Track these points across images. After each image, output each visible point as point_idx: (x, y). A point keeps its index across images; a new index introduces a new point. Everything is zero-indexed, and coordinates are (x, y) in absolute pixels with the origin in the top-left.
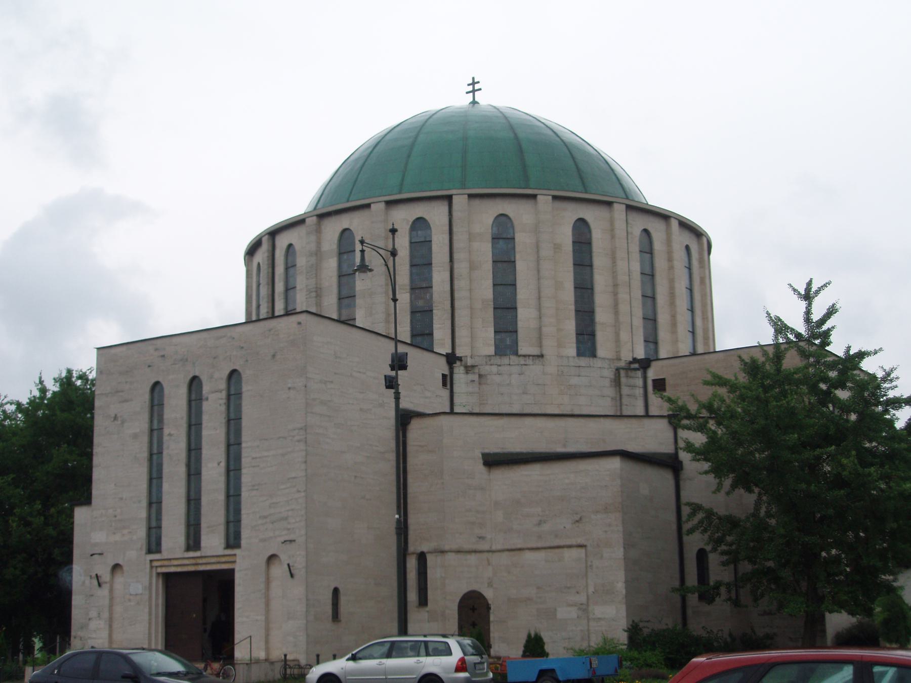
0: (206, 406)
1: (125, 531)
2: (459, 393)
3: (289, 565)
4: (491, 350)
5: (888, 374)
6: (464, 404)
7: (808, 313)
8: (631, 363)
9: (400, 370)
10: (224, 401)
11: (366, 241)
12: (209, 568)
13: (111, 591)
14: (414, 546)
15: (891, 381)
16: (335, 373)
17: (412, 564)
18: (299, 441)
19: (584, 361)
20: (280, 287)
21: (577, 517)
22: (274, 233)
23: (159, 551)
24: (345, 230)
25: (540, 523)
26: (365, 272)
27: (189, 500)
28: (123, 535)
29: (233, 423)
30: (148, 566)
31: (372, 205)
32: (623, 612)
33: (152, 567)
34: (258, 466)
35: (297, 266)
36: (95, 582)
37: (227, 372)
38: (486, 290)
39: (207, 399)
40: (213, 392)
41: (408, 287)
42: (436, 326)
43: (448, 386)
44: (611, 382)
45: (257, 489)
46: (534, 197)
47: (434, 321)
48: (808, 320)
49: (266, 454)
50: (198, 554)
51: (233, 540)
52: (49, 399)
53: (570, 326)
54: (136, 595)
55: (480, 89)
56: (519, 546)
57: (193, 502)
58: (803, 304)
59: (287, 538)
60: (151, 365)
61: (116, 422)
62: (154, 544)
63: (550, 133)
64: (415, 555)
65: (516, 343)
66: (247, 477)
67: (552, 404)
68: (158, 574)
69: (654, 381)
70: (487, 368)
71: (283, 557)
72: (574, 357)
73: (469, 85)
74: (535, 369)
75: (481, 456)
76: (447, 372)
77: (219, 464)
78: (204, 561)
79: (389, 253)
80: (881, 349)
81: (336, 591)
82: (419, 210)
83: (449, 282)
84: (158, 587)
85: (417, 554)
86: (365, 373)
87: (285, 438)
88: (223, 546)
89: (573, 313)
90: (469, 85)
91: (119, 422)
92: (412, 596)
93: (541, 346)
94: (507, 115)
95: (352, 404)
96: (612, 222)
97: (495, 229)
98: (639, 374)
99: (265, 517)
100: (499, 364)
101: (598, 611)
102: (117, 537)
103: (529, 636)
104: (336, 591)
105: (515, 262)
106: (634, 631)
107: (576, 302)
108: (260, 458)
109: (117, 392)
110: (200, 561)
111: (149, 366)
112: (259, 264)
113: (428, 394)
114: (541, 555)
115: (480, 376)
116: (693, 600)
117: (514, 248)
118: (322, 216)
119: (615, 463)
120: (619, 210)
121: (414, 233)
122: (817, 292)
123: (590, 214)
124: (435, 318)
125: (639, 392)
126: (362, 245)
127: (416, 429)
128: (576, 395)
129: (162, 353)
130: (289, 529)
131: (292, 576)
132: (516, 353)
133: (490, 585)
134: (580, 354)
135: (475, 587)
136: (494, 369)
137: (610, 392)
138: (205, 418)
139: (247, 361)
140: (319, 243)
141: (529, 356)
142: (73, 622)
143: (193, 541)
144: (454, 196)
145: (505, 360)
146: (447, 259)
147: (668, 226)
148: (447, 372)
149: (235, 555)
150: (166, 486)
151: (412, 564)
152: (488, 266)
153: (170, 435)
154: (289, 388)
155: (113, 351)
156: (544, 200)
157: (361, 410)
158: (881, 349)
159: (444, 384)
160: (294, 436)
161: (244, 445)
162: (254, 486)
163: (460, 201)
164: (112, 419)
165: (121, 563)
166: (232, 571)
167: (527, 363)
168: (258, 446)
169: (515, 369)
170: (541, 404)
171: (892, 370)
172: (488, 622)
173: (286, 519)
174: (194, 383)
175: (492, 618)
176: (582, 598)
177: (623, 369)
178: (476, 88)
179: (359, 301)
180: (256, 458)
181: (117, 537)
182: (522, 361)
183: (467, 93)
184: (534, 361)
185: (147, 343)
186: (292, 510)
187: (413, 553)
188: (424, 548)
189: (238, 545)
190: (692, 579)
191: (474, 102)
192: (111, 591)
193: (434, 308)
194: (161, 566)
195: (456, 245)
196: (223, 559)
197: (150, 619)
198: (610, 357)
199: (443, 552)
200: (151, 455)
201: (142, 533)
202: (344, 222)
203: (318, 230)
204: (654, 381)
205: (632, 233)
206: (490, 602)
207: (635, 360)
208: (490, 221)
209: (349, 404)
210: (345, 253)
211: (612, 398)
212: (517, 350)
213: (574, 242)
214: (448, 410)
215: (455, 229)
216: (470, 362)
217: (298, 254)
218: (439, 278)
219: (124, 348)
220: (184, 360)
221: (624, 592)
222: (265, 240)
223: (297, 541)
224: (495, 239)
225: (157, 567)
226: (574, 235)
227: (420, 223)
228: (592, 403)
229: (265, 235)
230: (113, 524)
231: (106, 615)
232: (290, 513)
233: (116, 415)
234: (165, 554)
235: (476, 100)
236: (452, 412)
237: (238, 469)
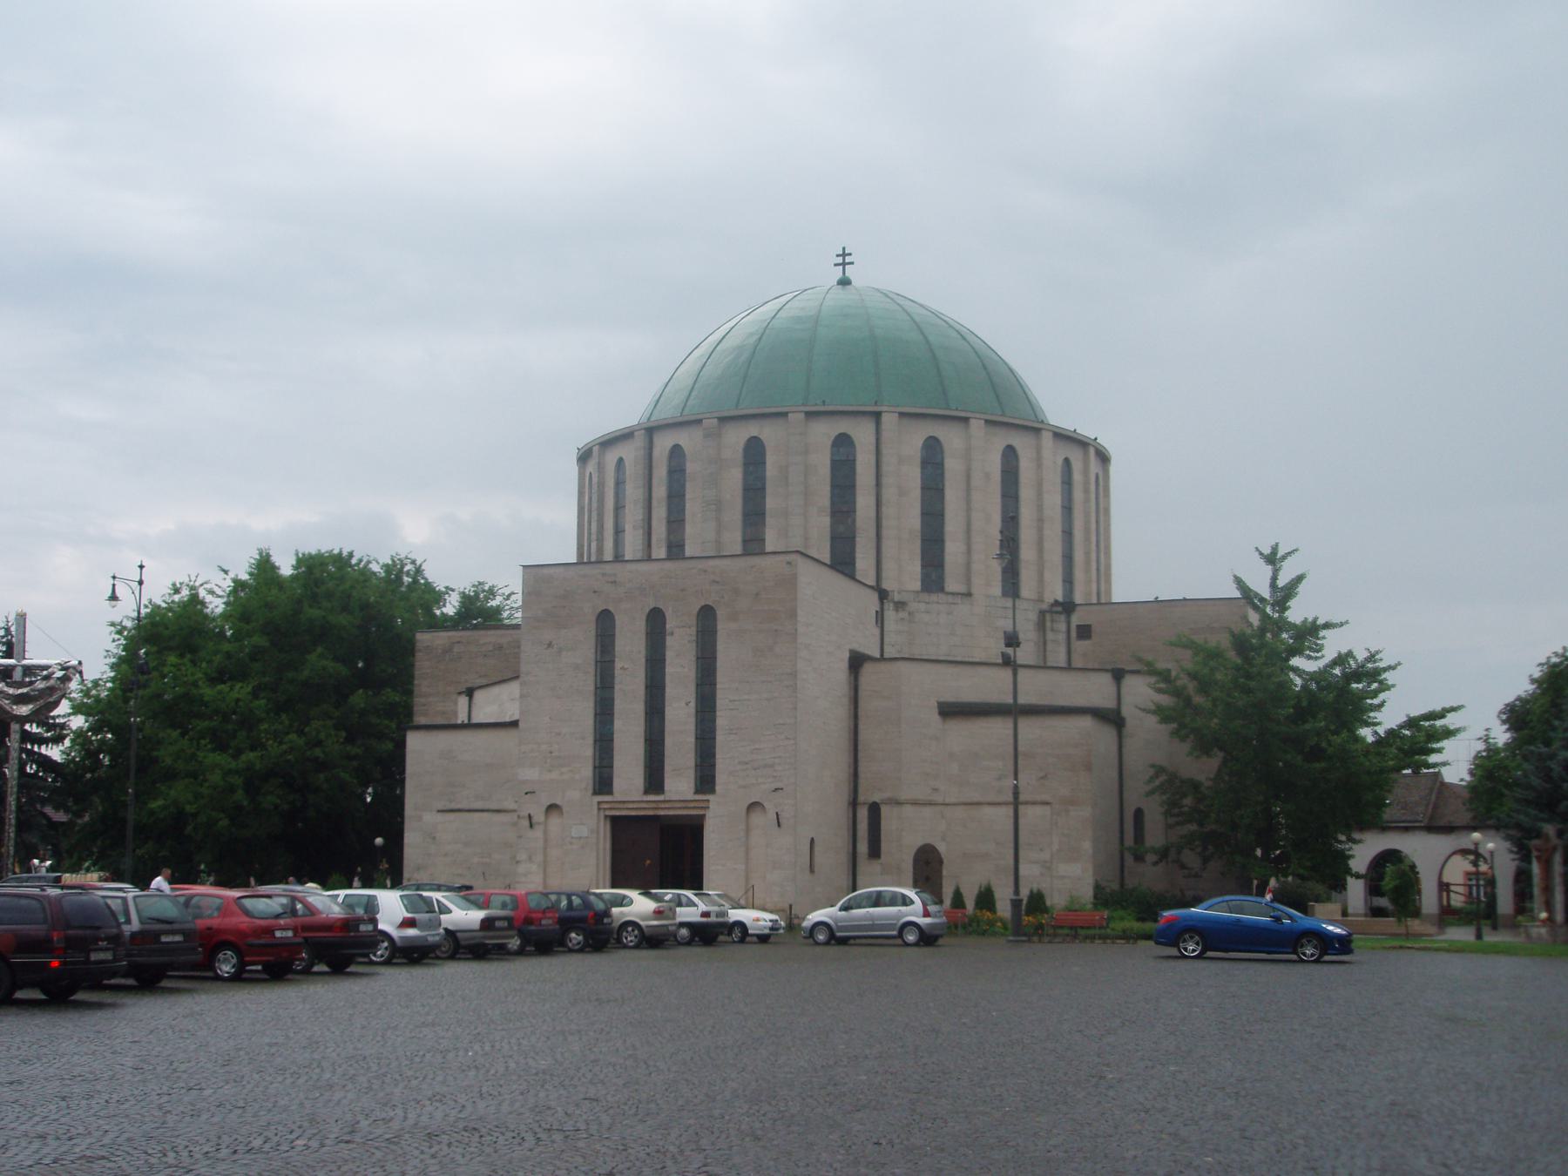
1: (564, 770)
4: (917, 585)
5: (1373, 656)
7: (1274, 578)
12: (671, 813)
13: (545, 832)
14: (867, 795)
15: (1375, 662)
17: (863, 814)
18: (787, 687)
20: (660, 492)
21: (1042, 774)
23: (610, 792)
25: (999, 779)
28: (562, 774)
30: (596, 807)
31: (790, 415)
32: (1090, 872)
33: (599, 809)
36: (526, 823)
38: (914, 521)
42: (859, 555)
43: (879, 625)
45: (736, 734)
46: (966, 420)
48: (1273, 585)
49: (746, 697)
50: (661, 798)
51: (706, 781)
52: (442, 613)
54: (580, 838)
55: (852, 263)
56: (975, 800)
58: (1269, 569)
62: (603, 783)
63: (955, 334)
66: (722, 721)
68: (606, 817)
69: (1079, 627)
73: (838, 256)
75: (936, 704)
77: (687, 704)
78: (667, 805)
80: (1347, 622)
81: (812, 840)
82: (843, 426)
83: (875, 508)
84: (605, 830)
88: (693, 790)
90: (838, 256)
92: (863, 847)
94: (917, 319)
98: (1063, 617)
101: (1064, 869)
102: (554, 775)
103: (1031, 892)
104: (812, 840)
106: (1098, 888)
108: (739, 700)
110: (663, 805)
112: (621, 460)
115: (909, 613)
116: (1129, 859)
118: (723, 420)
119: (1086, 722)
120: (1047, 438)
122: (1284, 558)
123: (1021, 442)
125: (1062, 637)
130: (775, 777)
131: (779, 825)
133: (943, 839)
135: (928, 841)
136: (922, 606)
142: (406, 862)
143: (654, 780)
144: (883, 414)
145: (934, 597)
146: (874, 483)
147: (1086, 453)
149: (708, 801)
152: (916, 493)
155: (546, 571)
156: (976, 426)
158: (1347, 622)
162: (731, 730)
163: (889, 420)
164: (546, 646)
165: (558, 802)
166: (703, 817)
171: (1377, 652)
172: (940, 877)
173: (772, 766)
175: (945, 873)
176: (1046, 856)
178: (847, 261)
179: (769, 520)
180: (734, 701)
181: (554, 775)
182: (950, 599)
183: (836, 265)
186: (780, 757)
187: (864, 804)
188: (876, 798)
189: (712, 791)
190: (1129, 841)
192: (545, 832)
194: (611, 809)
195: (885, 468)
196: (692, 805)
197: (598, 865)
198: (1033, 597)
199: (899, 803)
201: (587, 772)
206: (943, 856)
207: (1056, 603)
216: (897, 598)
218: (864, 503)
219: (561, 569)
221: (1091, 851)
222: (640, 436)
225: (605, 809)
227: (843, 443)
229: (641, 430)
230: (548, 761)
231: (539, 858)
232: (777, 761)
235: (847, 274)
237: (713, 709)
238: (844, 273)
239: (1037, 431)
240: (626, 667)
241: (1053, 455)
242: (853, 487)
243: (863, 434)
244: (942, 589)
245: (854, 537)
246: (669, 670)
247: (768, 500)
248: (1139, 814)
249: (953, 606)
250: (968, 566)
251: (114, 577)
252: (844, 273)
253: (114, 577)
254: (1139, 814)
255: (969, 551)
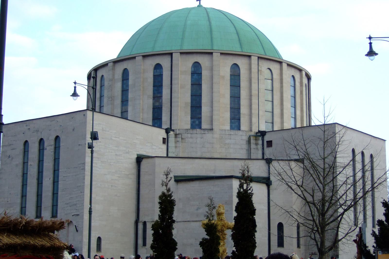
0: (45, 152)
1: (12, 209)
2: (171, 147)
3: (75, 226)
4: (189, 127)
6: (174, 152)
8: (257, 133)
9: (94, 140)
10: (53, 150)
11: (77, 83)
16: (102, 138)
17: (140, 226)
19: (233, 132)
22: (96, 70)
24: (126, 69)
26: (372, 56)
27: (38, 195)
29: (56, 160)
31: (136, 57)
34: (65, 180)
35: (105, 86)
37: (54, 137)
38: (187, 98)
39: (46, 149)
40: (48, 146)
41: (152, 96)
44: (246, 142)
45: (65, 191)
46: (211, 53)
47: (163, 113)
49: (69, 175)
53: (227, 115)
56: (188, 220)
57: (39, 196)
59: (76, 214)
60: (24, 133)
61: (10, 159)
64: (142, 223)
65: (200, 123)
66: (61, 186)
67: (216, 152)
69: (267, 142)
70: (186, 135)
71: (74, 223)
72: (228, 130)
74: (208, 136)
76: (166, 137)
79: (92, 88)
82: (157, 60)
85: (143, 222)
86: (119, 138)
87: (76, 168)
89: (229, 109)
91: (11, 159)
92: (140, 241)
93: (212, 125)
95: (112, 152)
96: (250, 65)
97: (193, 69)
99: (67, 204)
100: (192, 133)
105: (201, 84)
107: (231, 104)
108: (66, 176)
109: (10, 145)
111: (23, 133)
113: (154, 147)
114: (195, 223)
117: (201, 78)
121: (155, 71)
124: (163, 111)
126: (370, 40)
127: (144, 163)
128: (229, 148)
129: (28, 127)
130: (77, 210)
131: (77, 231)
132: (200, 128)
134: (232, 128)
136: (189, 135)
137: (245, 146)
138: (45, 157)
139: (63, 132)
140: (113, 75)
141: (206, 129)
143: (39, 215)
144: (173, 53)
145: (195, 131)
148: (166, 137)
150: (28, 188)
151: (140, 226)
152: (189, 86)
153: (31, 165)
154: (79, 145)
157: (116, 155)
159: (164, 142)
160: (80, 167)
161: (60, 170)
162: (63, 189)
164: (8, 157)
167: (205, 132)
168: (66, 171)
169: (199, 136)
170: (211, 152)
173: (76, 205)
174: (41, 141)
177: (252, 136)
180: (65, 177)
184: (209, 132)
185: (23, 122)
191: (200, 6)
193: (163, 106)
200: (23, 174)
202: (125, 65)
203: (113, 69)
204: (267, 142)
205: (261, 70)
207: (259, 132)
208: (191, 65)
209: (109, 152)
210: (124, 80)
211: (247, 150)
212: (201, 127)
213: (231, 75)
214: (165, 156)
215: (173, 69)
217: (105, 80)
218: (166, 92)
219: (14, 125)
220: (37, 131)
223: (80, 215)
224: (193, 74)
226: (231, 71)
228: (236, 152)
233: (9, 155)
234: (44, 219)
235: (201, 4)
236: (167, 157)
238: (200, 3)
239: (280, 63)
240: (31, 164)
241: (288, 73)
242: (161, 86)
243: (165, 62)
244: (240, 130)
245: (162, 108)
246: (45, 164)
247: (129, 94)
248: (280, 226)
249: (203, 134)
250: (212, 117)
251: (75, 83)
252: (200, 3)
253: (75, 83)
254: (280, 226)
255: (212, 111)
